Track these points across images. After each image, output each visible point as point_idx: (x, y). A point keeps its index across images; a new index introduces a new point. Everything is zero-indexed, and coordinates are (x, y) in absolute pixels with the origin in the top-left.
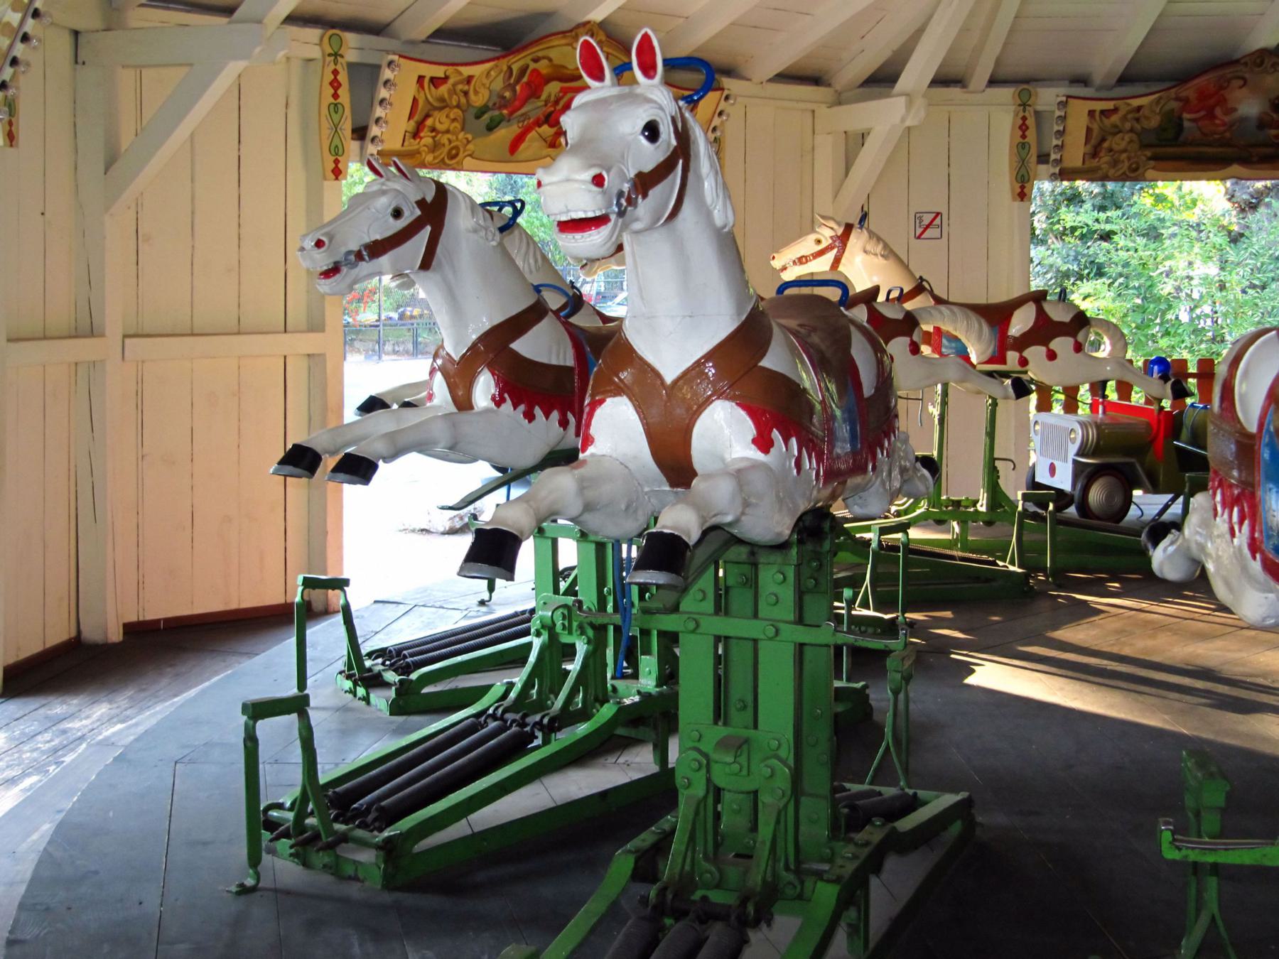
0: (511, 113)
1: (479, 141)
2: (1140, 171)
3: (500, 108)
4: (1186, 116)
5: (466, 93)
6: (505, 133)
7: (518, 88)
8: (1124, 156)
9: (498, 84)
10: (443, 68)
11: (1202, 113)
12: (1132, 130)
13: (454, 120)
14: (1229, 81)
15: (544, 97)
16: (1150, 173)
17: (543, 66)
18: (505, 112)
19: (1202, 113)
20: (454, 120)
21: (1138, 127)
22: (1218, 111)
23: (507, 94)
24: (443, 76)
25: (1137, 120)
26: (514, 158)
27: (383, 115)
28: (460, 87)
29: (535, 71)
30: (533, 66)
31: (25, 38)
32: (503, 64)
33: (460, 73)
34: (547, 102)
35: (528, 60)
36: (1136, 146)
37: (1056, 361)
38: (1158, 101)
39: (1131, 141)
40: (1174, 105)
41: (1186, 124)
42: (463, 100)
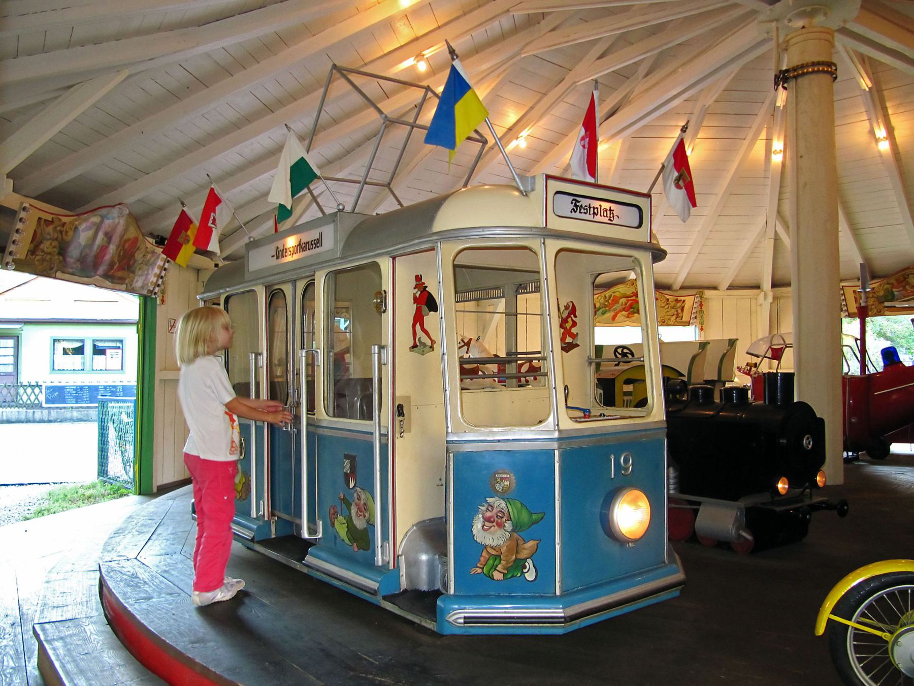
0: (610, 309)
1: (600, 318)
2: (882, 312)
3: (605, 307)
4: (894, 290)
5: (61, 232)
6: (610, 315)
7: (610, 301)
8: (873, 307)
9: (602, 301)
10: (52, 216)
11: (901, 288)
12: (873, 297)
13: (54, 247)
14: (908, 275)
15: (620, 303)
16: (886, 313)
17: (617, 294)
18: (607, 309)
19: (901, 288)
20: (54, 247)
21: (875, 295)
22: (907, 287)
23: (606, 303)
24: (51, 220)
25: (874, 293)
26: (615, 321)
27: (14, 250)
28: (59, 228)
29: (614, 296)
30: (613, 294)
31: (165, 269)
32: (603, 295)
33: (60, 220)
34: (622, 304)
35: (611, 293)
36: (877, 303)
37: (400, 403)
38: (880, 285)
39: (874, 301)
40: (887, 286)
41: (895, 293)
42: (60, 236)
